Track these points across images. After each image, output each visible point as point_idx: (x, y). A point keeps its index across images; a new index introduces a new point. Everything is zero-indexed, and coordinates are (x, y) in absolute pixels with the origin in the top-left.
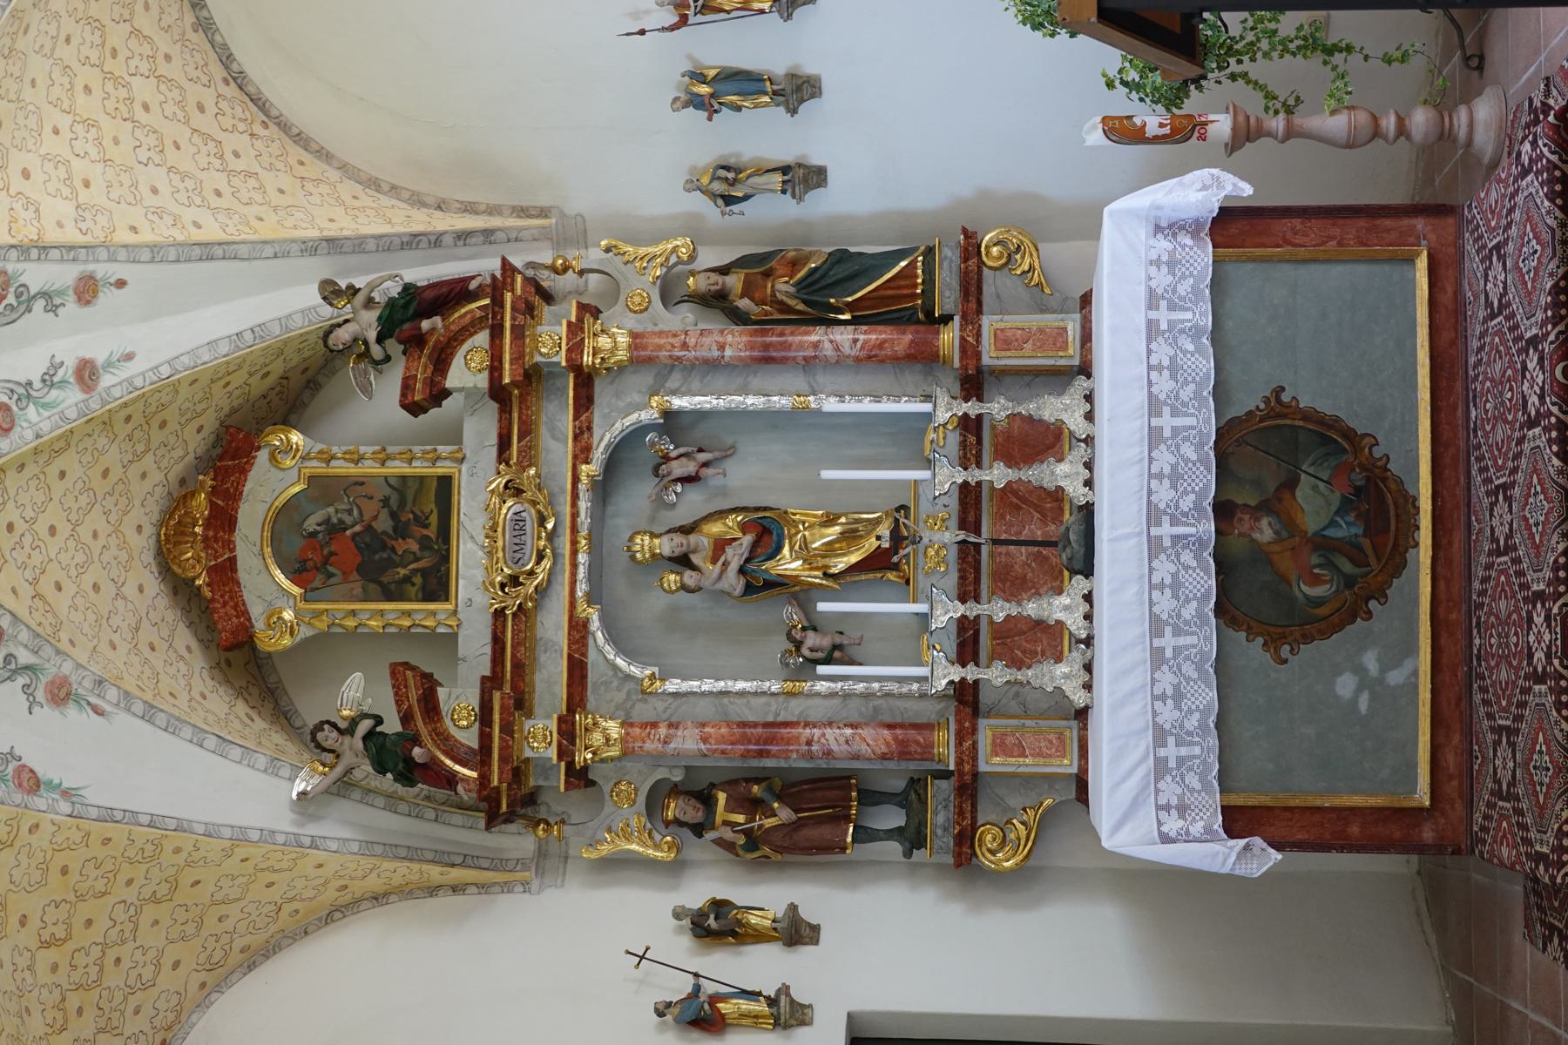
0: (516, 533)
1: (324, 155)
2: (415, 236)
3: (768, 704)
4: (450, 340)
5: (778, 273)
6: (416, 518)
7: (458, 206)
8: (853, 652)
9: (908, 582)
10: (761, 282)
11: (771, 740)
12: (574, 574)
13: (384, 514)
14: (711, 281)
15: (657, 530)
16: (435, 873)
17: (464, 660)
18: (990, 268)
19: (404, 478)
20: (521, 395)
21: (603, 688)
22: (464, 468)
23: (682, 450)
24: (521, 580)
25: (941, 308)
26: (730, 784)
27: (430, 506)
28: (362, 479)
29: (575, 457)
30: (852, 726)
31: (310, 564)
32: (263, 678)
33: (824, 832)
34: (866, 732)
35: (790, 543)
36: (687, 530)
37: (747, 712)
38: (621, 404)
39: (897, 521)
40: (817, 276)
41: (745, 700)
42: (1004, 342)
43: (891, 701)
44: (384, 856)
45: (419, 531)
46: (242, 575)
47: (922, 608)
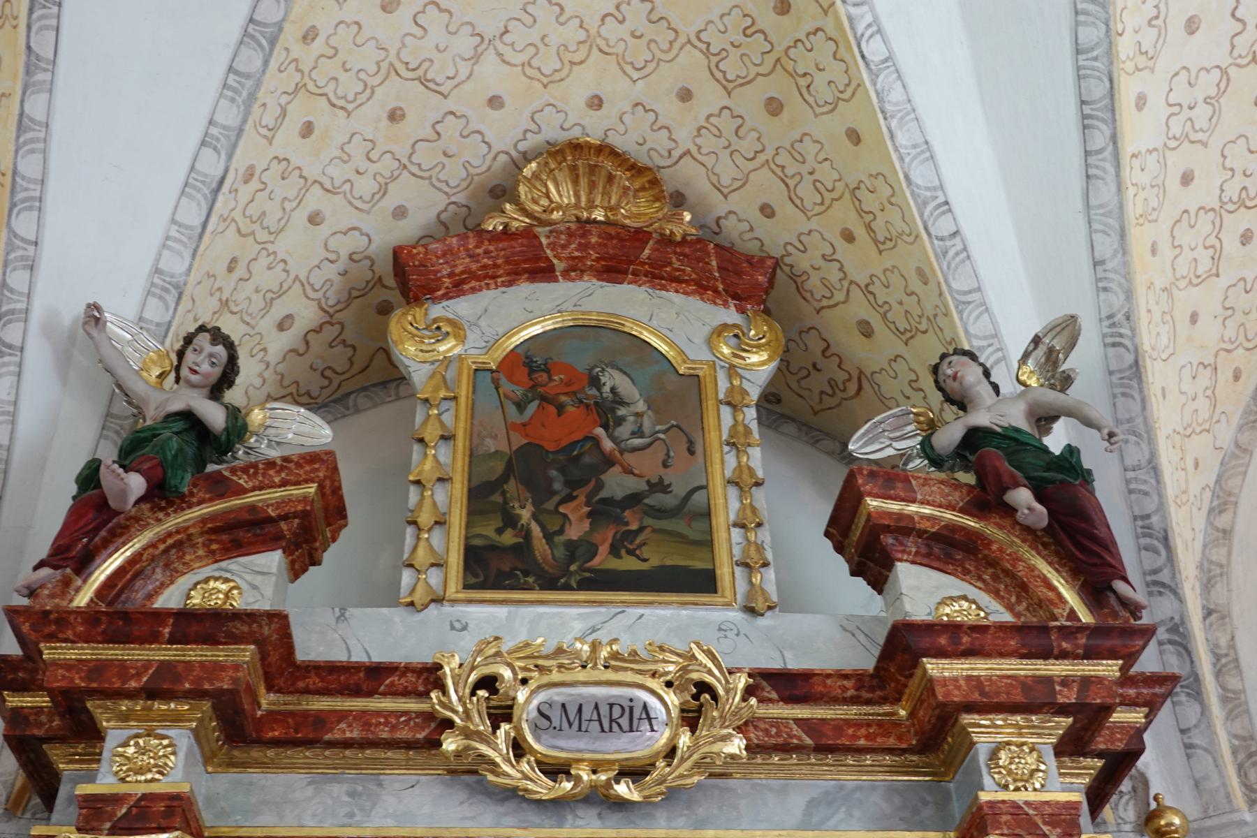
0: (604, 710)
2: (1166, 540)
4: (993, 563)
7: (1223, 641)
13: (634, 485)
19: (707, 514)
20: (897, 724)
22: (735, 615)
24: (505, 727)
27: (655, 557)
28: (699, 449)
31: (543, 377)
32: (364, 389)
46: (525, 289)
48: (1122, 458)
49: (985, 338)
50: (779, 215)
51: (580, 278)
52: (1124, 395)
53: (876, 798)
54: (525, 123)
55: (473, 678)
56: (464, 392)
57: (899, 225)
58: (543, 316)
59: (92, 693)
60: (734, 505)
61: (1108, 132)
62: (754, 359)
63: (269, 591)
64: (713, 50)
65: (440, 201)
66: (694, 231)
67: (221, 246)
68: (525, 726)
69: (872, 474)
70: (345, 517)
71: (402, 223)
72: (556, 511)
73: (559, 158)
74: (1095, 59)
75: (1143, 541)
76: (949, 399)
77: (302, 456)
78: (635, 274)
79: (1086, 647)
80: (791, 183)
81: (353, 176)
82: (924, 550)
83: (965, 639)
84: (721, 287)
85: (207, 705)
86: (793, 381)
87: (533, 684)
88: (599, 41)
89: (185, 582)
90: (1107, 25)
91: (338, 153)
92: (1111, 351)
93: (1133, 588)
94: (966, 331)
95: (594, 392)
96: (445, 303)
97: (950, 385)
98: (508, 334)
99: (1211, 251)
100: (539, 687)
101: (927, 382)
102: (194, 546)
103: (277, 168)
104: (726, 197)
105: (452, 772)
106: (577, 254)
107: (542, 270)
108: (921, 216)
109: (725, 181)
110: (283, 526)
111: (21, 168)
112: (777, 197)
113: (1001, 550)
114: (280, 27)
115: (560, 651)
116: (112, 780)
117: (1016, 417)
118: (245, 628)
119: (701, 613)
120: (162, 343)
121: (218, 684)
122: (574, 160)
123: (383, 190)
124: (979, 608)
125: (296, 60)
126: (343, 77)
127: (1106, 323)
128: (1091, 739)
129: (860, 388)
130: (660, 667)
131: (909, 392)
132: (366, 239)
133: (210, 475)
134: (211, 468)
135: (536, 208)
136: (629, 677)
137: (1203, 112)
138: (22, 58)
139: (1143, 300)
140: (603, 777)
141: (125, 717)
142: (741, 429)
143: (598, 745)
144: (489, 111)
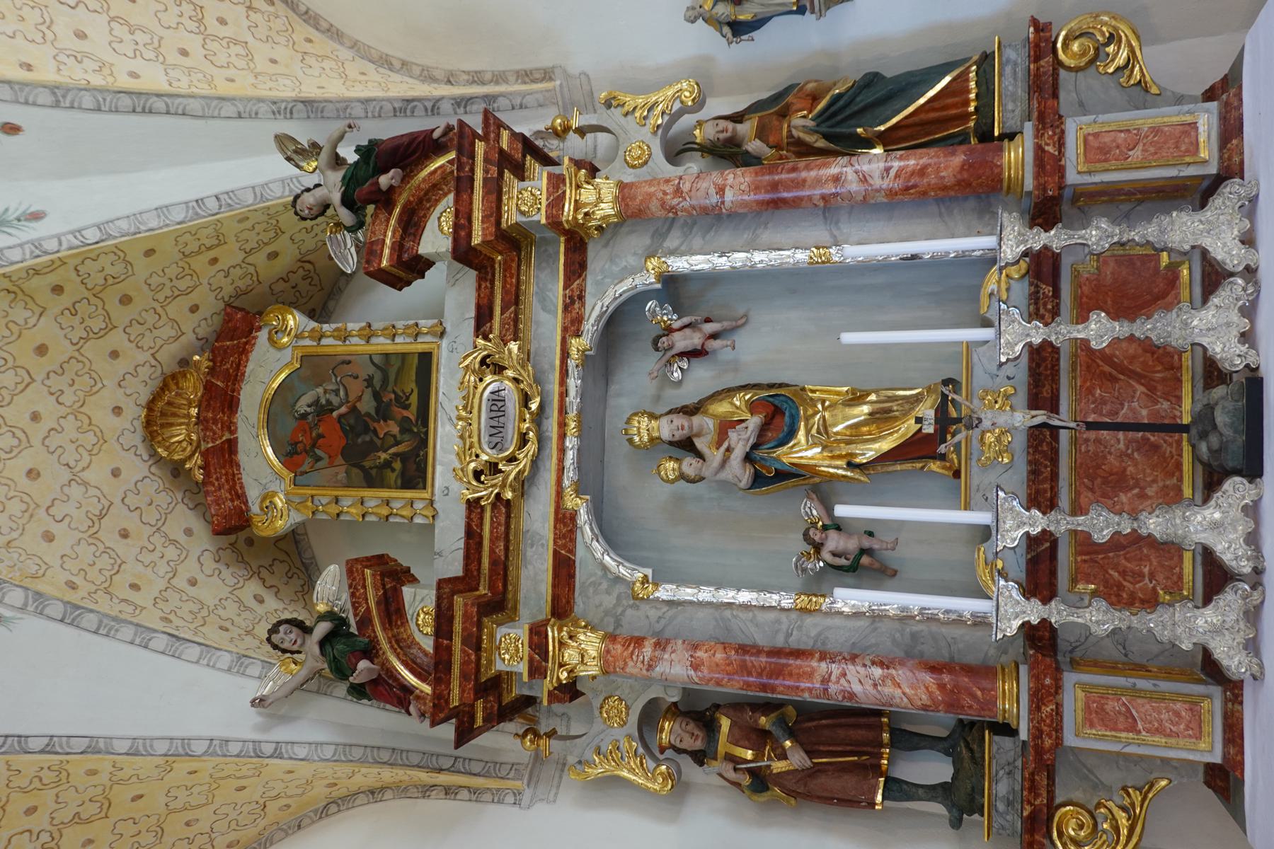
0: (494, 414)
1: (334, 33)
2: (408, 101)
3: (778, 621)
4: (420, 201)
5: (794, 108)
6: (397, 398)
7: (465, 77)
8: (891, 558)
9: (957, 474)
10: (776, 123)
11: (778, 672)
12: (561, 460)
13: (368, 396)
14: (720, 128)
15: (659, 410)
16: (424, 777)
17: (440, 554)
18: (1069, 69)
19: (387, 356)
20: (505, 261)
21: (591, 590)
22: (445, 343)
23: (686, 320)
24: (500, 466)
25: (1002, 122)
26: (736, 706)
27: (411, 385)
28: (348, 358)
29: (565, 329)
30: (882, 664)
32: (299, 554)
33: (848, 784)
34: (900, 674)
35: (806, 425)
36: (690, 411)
37: (753, 629)
38: (616, 269)
39: (944, 397)
40: (841, 103)
41: (751, 614)
42: (1097, 151)
43: (934, 627)
44: (362, 761)
45: (398, 412)
46: (242, 457)
47: (982, 517)
48: (360, 118)
49: (284, 187)
50: (197, 302)
51: (235, 424)
52: (322, 112)
53: (543, 276)
54: (131, 454)
55: (474, 483)
56: (309, 492)
57: (210, 231)
58: (261, 447)
59: (477, 679)
60: (382, 340)
61: (155, 99)
62: (291, 323)
63: (425, 592)
64: (85, 335)
65: (181, 507)
66: (206, 354)
67: (212, 634)
68: (500, 456)
69: (368, 262)
70: (383, 555)
71: (195, 531)
72: (383, 439)
73: (155, 434)
74: (104, 100)
75: (408, 113)
76: (322, 213)
77: (349, 577)
78: (233, 391)
79: (468, 158)
80: (177, 293)
81: (165, 560)
82: (412, 238)
83: (462, 221)
84: (244, 340)
85: (485, 620)
86: (302, 301)
87: (479, 451)
88: (76, 406)
89: (418, 637)
90: (81, 90)
91: (149, 569)
92: (295, 115)
93: (436, 124)
94: (279, 198)
95: (310, 417)
96: (250, 504)
97: (315, 212)
98: (271, 467)
99: (231, 45)
100: (480, 448)
101: (309, 223)
102: (398, 634)
103: (161, 604)
104: (183, 334)
105: (523, 495)
106: (219, 426)
107: (230, 447)
108: (205, 217)
109: (173, 333)
110: (388, 586)
111: (163, 752)
112: (185, 302)
113: (413, 196)
114: (66, 603)
115: (462, 437)
116: (521, 665)
117: (336, 177)
118: (445, 601)
119: (443, 361)
120: (275, 665)
121: (475, 614)
122: (157, 426)
123: (174, 542)
124: (445, 211)
125: (89, 594)
126: (98, 566)
127: (278, 116)
128: (516, 160)
129: (309, 262)
130: (472, 384)
131: (313, 234)
132: (206, 553)
133: (359, 629)
134: (354, 630)
135: (189, 449)
136: (476, 401)
137: (139, 37)
138: (89, 756)
139: (263, 92)
140: (528, 416)
141: (490, 662)
142: (336, 334)
143: (511, 418)
144: (122, 477)
